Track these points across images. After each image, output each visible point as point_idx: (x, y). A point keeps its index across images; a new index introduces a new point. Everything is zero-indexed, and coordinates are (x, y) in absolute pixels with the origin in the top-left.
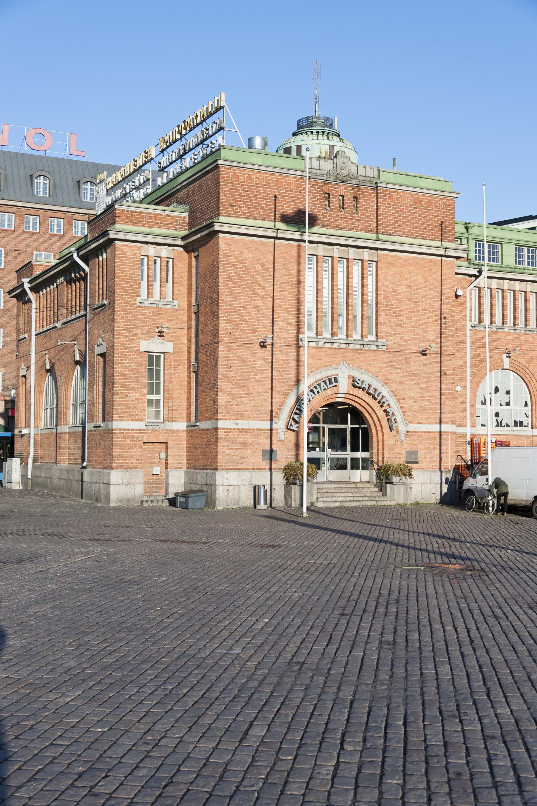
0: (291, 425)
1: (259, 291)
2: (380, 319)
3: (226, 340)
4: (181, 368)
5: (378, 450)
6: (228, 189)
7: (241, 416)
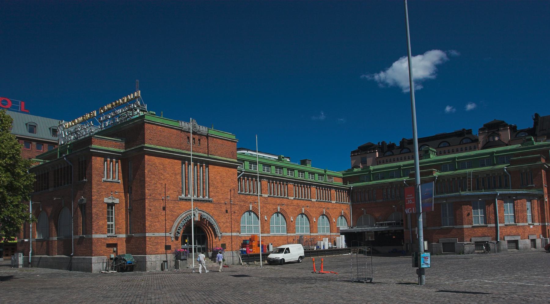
0: (177, 235)
1: (162, 177)
2: (210, 190)
3: (149, 198)
4: (122, 210)
5: (210, 244)
6: (148, 132)
7: (156, 231)
